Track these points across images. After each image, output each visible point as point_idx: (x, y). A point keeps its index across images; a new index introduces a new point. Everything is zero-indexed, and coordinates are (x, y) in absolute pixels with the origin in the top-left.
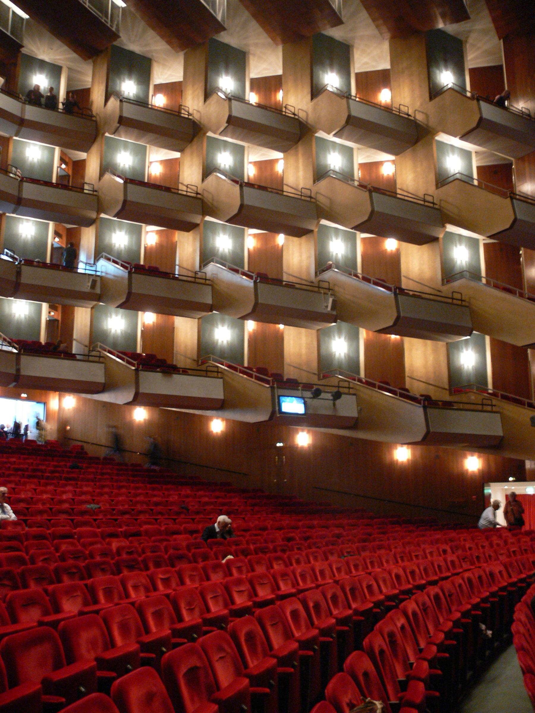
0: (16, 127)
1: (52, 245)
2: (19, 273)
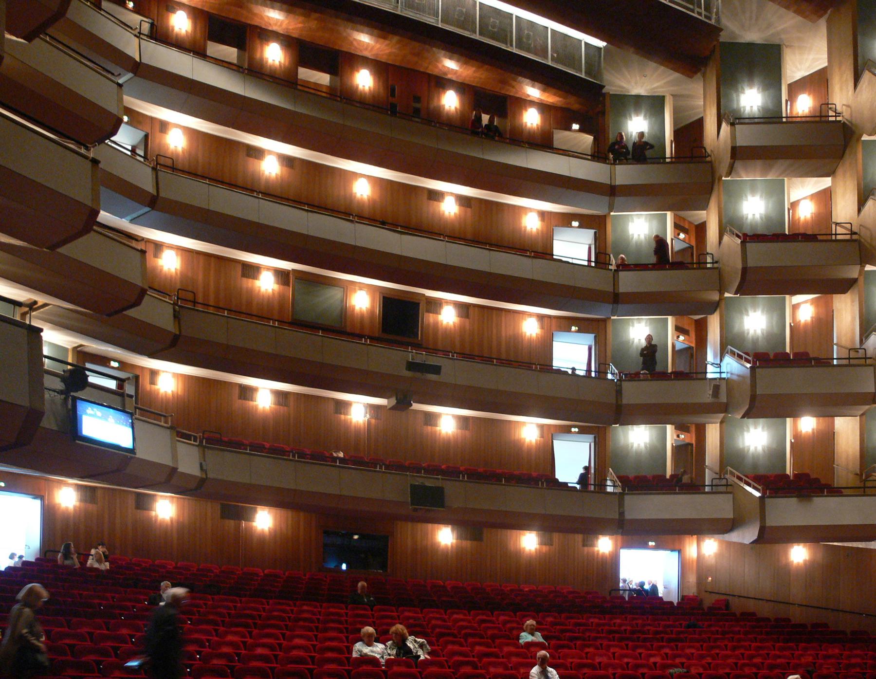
0: (606, 199)
1: (673, 346)
2: (619, 392)
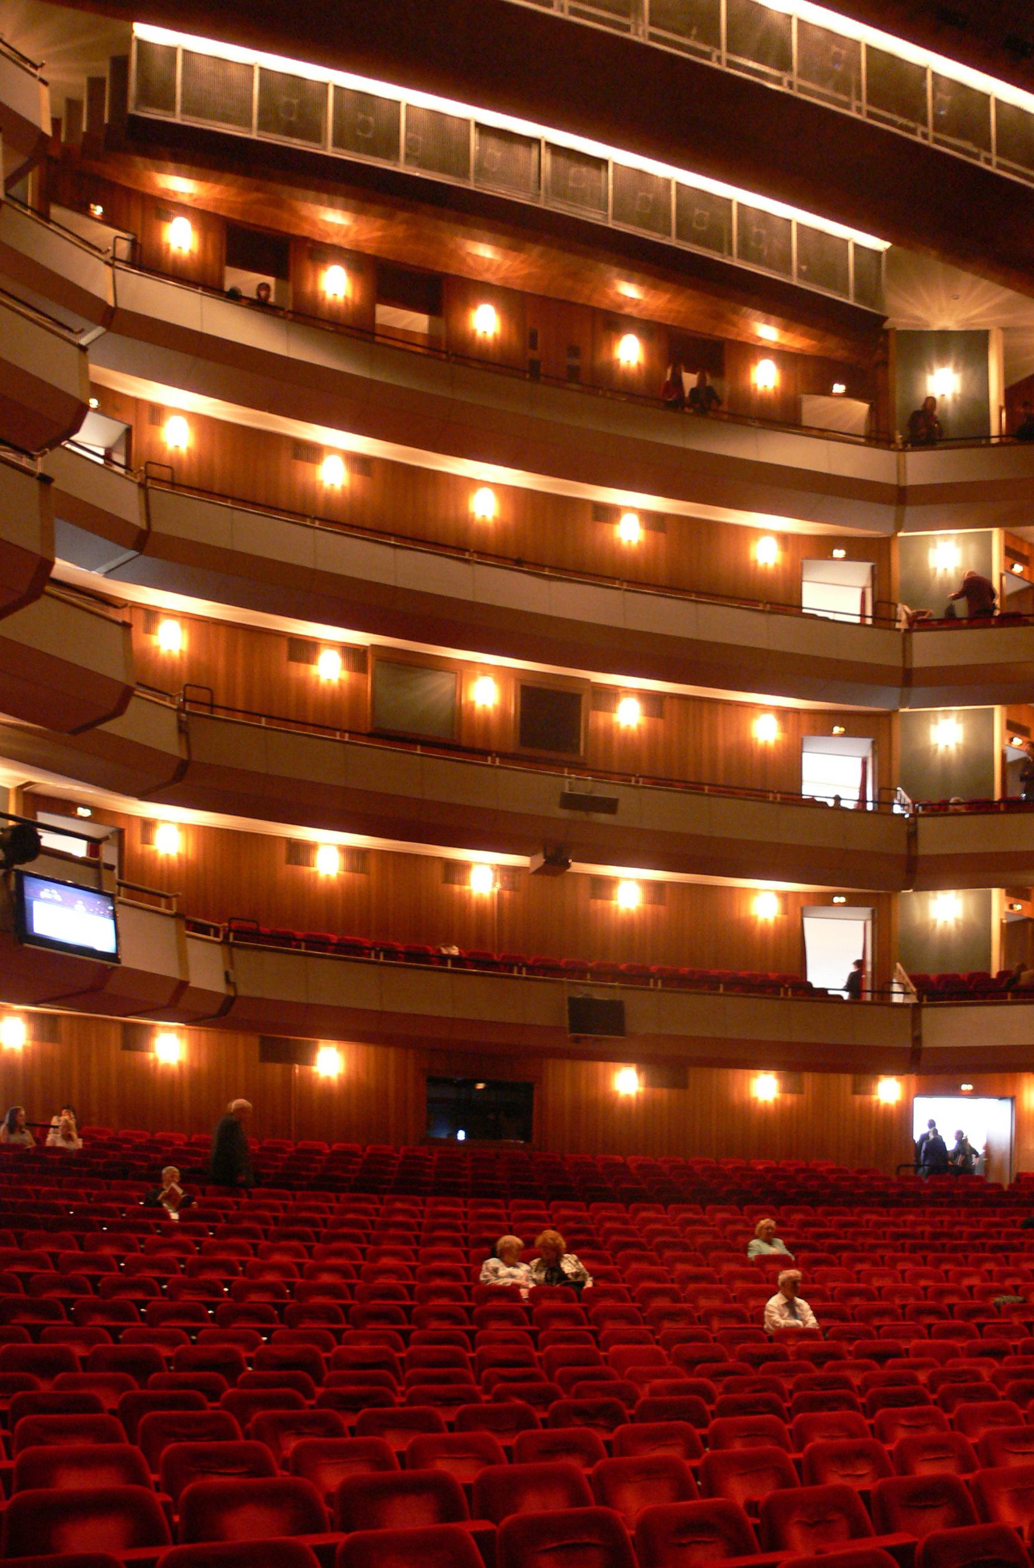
1: (1004, 756)
2: (912, 836)
